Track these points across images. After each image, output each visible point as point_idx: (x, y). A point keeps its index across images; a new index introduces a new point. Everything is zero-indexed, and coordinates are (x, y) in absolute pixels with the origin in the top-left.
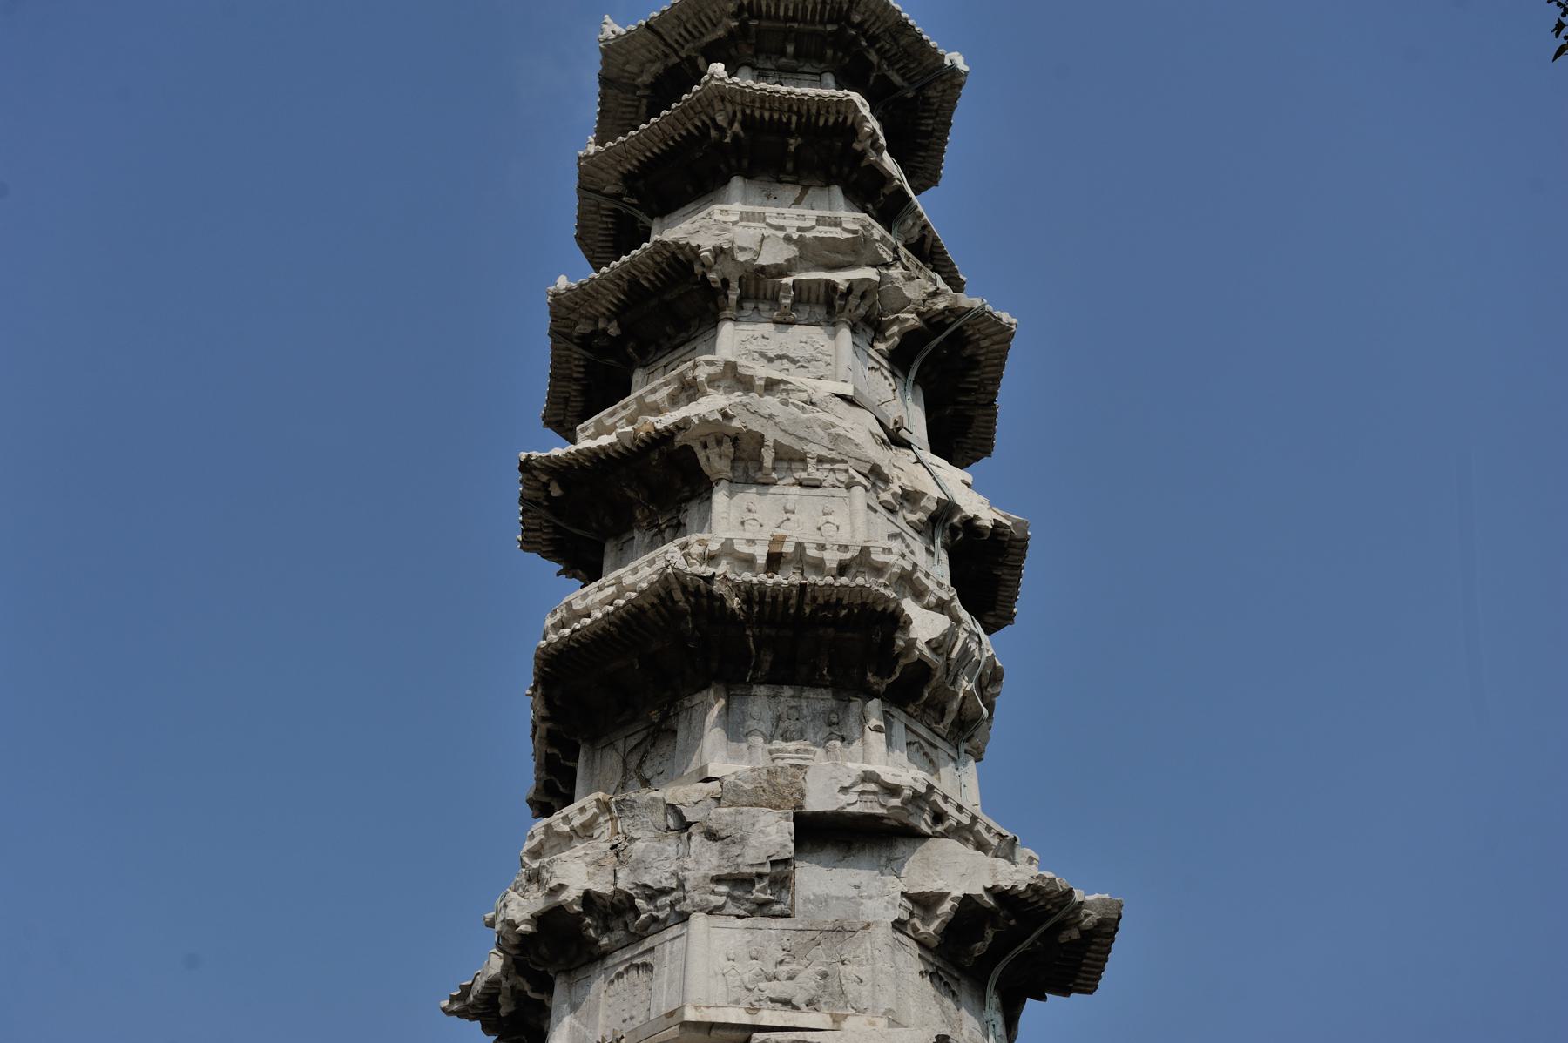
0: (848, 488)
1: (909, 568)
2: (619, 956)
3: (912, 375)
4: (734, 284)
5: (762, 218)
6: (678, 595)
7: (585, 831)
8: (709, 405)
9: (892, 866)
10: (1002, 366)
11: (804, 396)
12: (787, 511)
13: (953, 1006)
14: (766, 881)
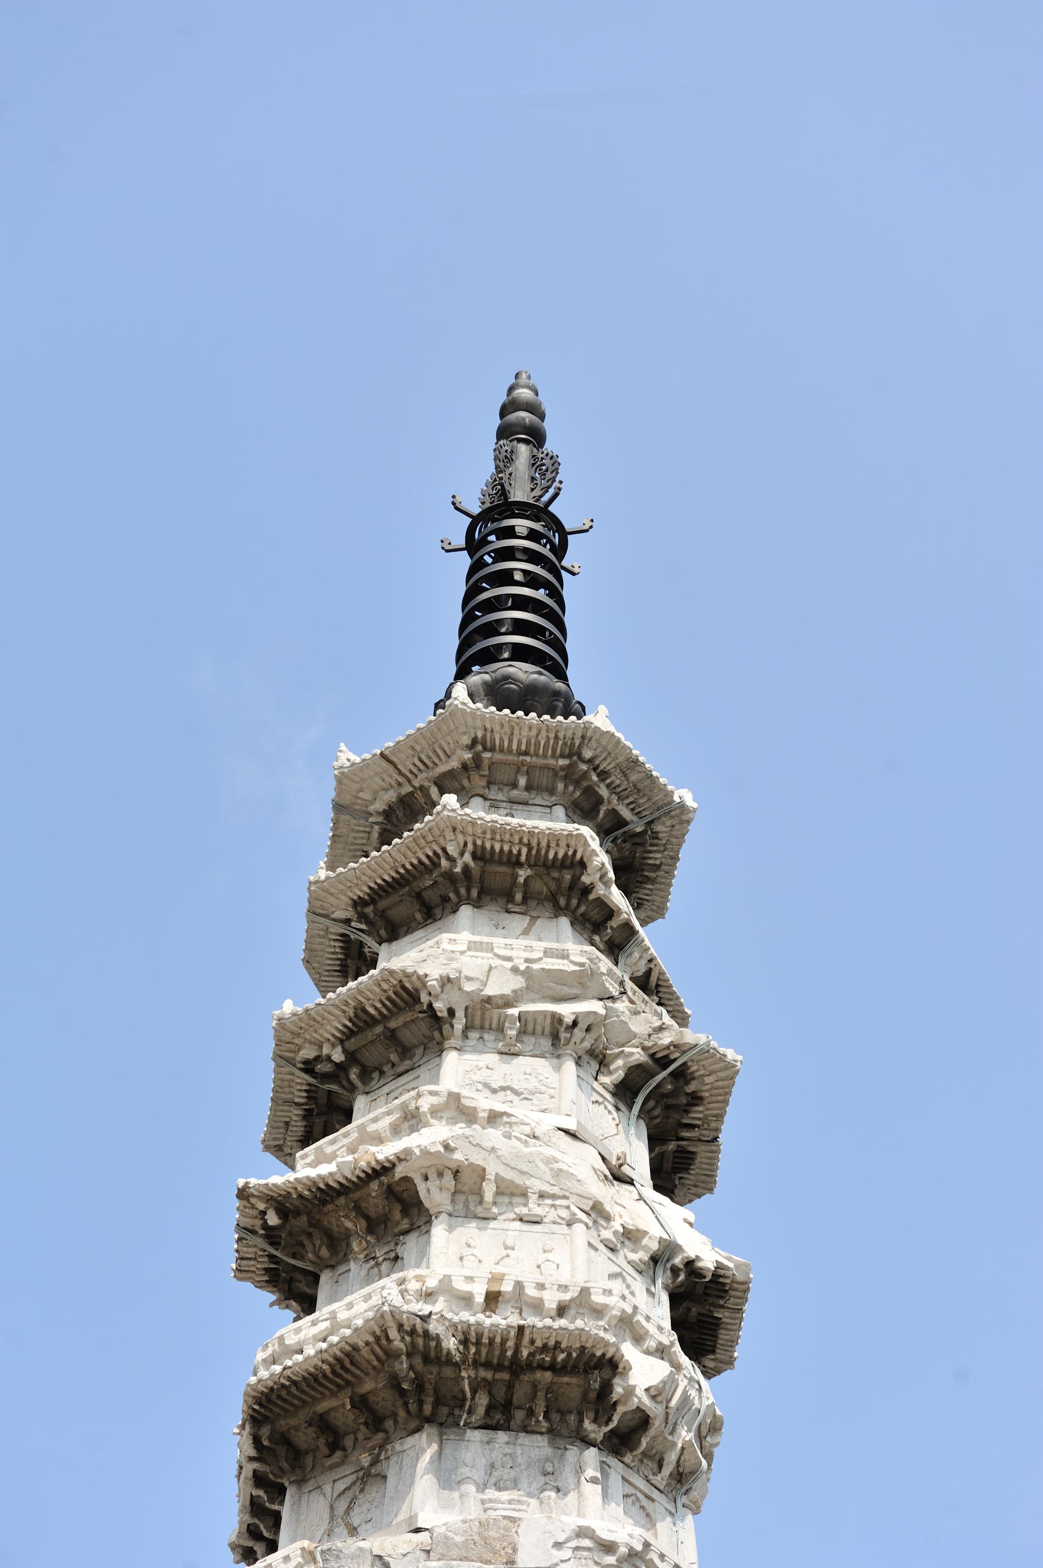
0: (569, 1225)
1: (630, 1311)
5: (489, 948)
6: (393, 1334)
8: (430, 1137)
10: (726, 1102)
11: (527, 1130)
12: (506, 1248)
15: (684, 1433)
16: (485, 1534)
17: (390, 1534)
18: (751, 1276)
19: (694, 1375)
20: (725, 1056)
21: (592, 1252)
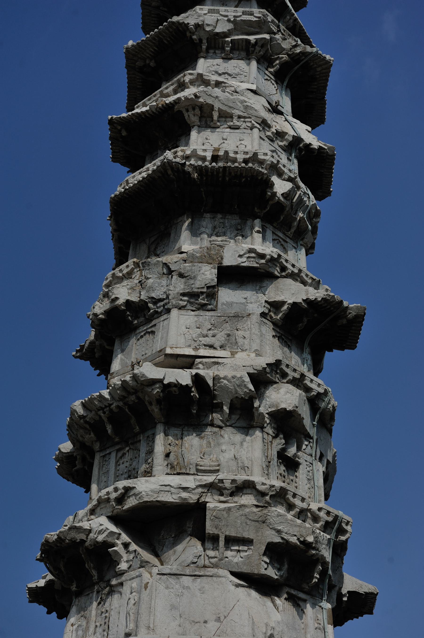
0: (251, 129)
1: (275, 162)
3: (285, 84)
4: (205, 41)
5: (218, 12)
6: (170, 172)
7: (129, 275)
8: (189, 92)
9: (262, 289)
10: (327, 80)
11: (233, 89)
12: (223, 139)
13: (288, 351)
14: (205, 295)
15: (300, 214)
16: (209, 253)
17: (171, 255)
18: (335, 152)
19: (306, 191)
20: (325, 58)
21: (262, 141)
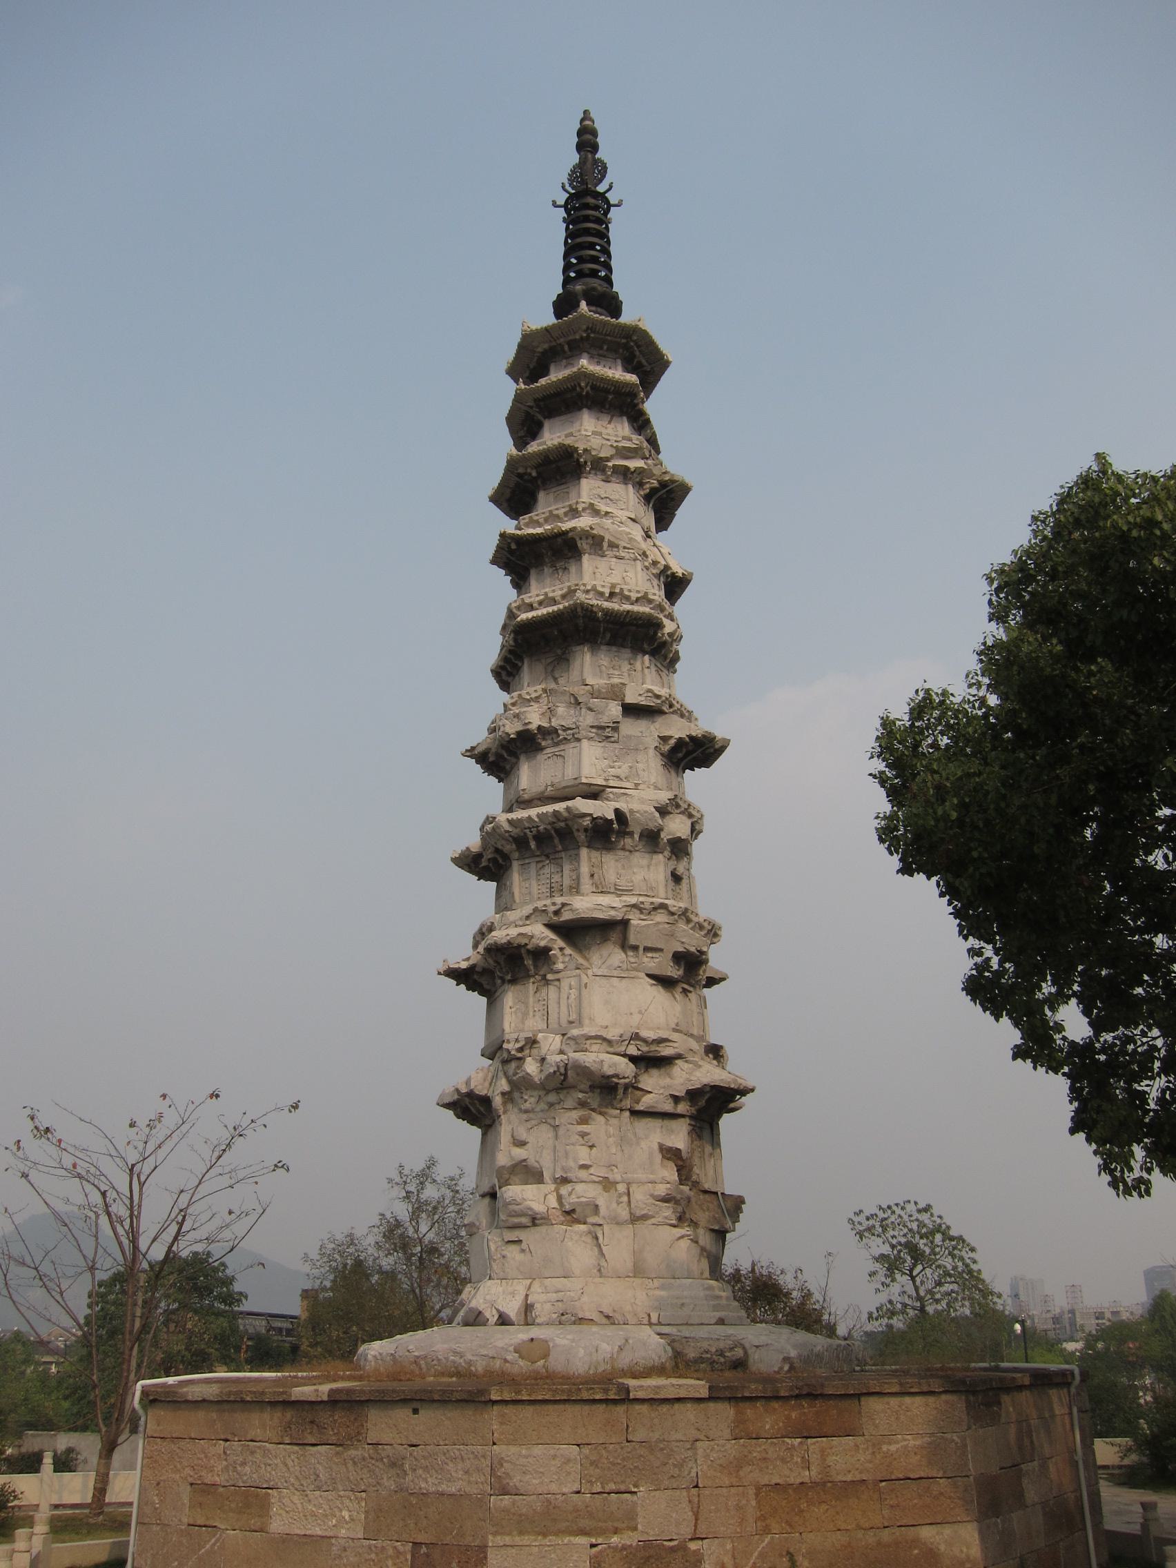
2: (548, 750)
